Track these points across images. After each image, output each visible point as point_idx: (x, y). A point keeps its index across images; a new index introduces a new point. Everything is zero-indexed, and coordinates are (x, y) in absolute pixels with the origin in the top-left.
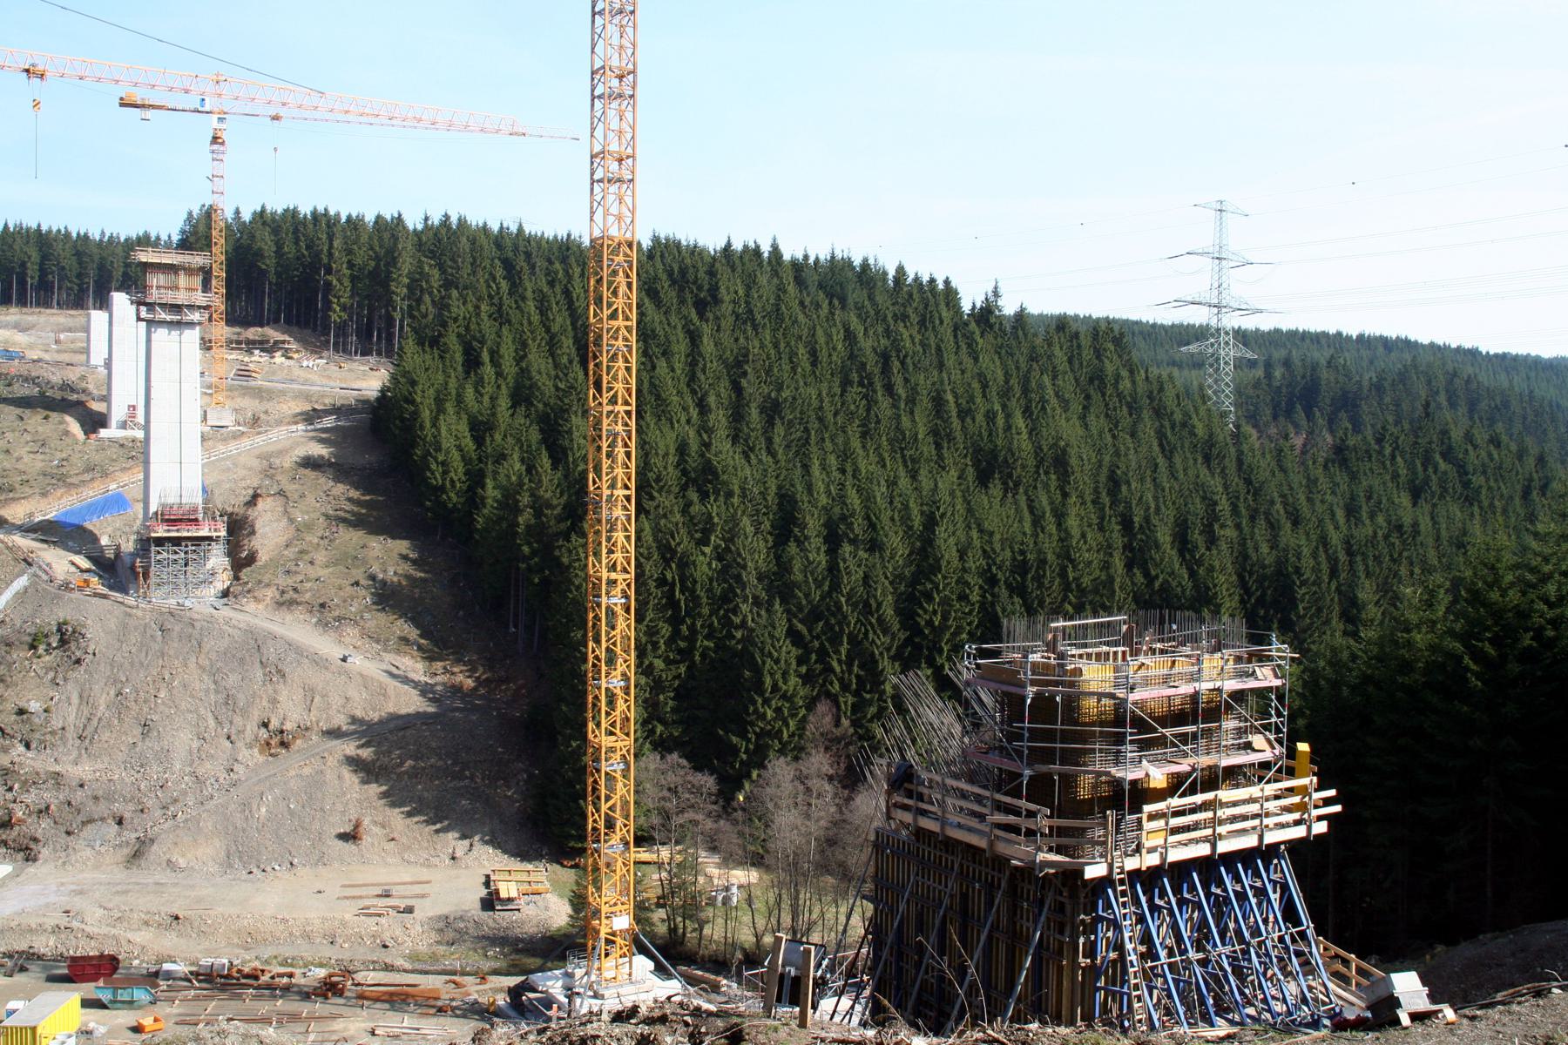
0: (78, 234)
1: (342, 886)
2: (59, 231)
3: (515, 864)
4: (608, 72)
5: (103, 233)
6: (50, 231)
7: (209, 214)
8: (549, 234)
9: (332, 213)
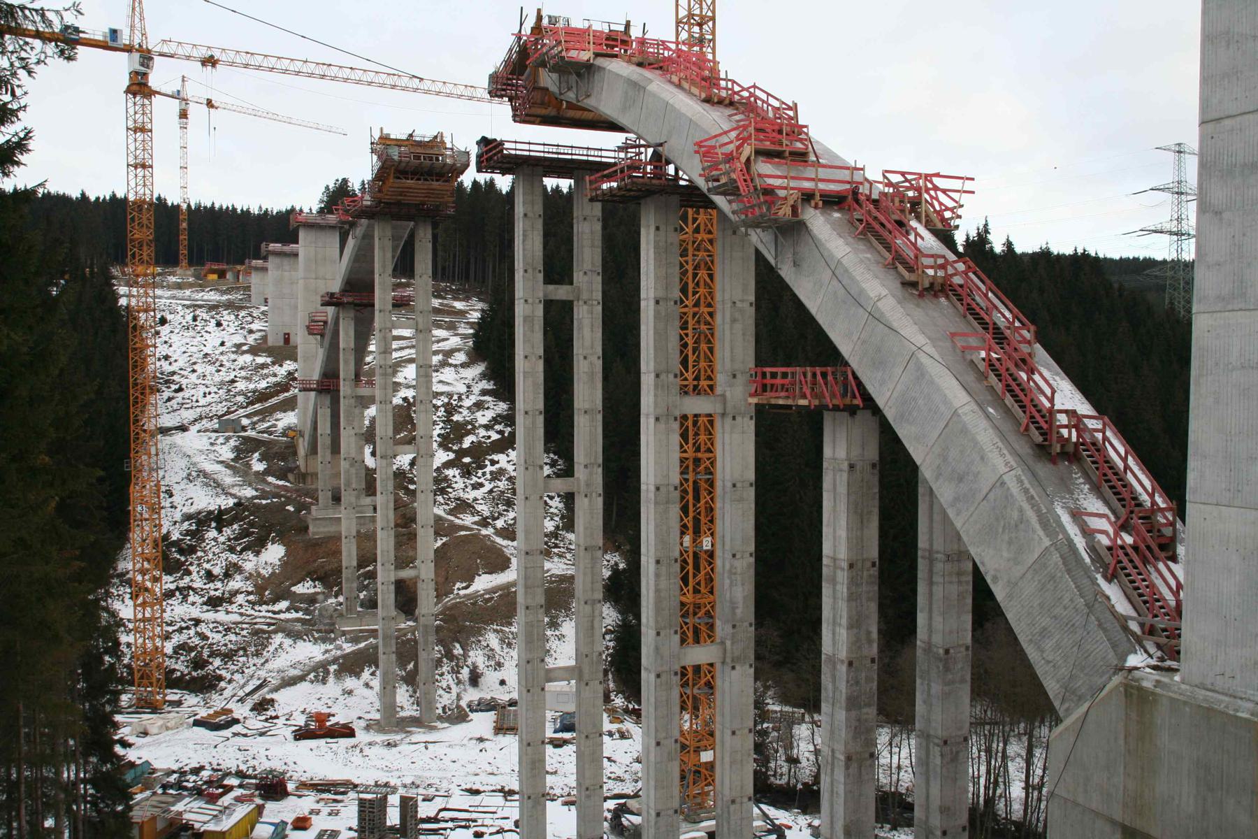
0: (242, 210)
2: (228, 208)
6: (221, 208)
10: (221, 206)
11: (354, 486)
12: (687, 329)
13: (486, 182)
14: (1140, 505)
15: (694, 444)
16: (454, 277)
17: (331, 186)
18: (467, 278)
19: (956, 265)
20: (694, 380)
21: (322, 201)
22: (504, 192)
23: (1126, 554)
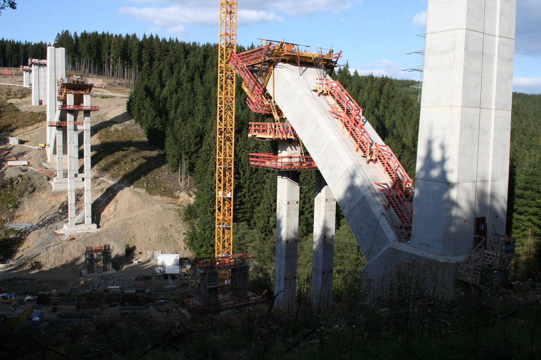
1: (76, 224)
2: (10, 41)
10: (7, 40)
11: (73, 169)
12: (223, 73)
13: (132, 35)
14: (51, 189)
15: (224, 153)
16: (117, 77)
17: (60, 34)
18: (124, 77)
19: (333, 84)
20: (225, 126)
21: (56, 40)
22: (140, 40)
23: (393, 199)
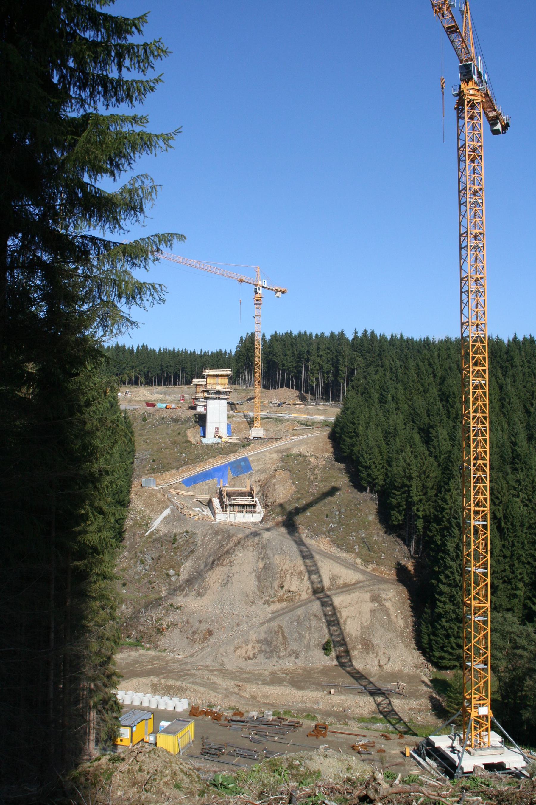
3: (297, 691)
4: (469, 235)
5: (201, 351)
7: (251, 338)
8: (416, 338)
9: (308, 333)
